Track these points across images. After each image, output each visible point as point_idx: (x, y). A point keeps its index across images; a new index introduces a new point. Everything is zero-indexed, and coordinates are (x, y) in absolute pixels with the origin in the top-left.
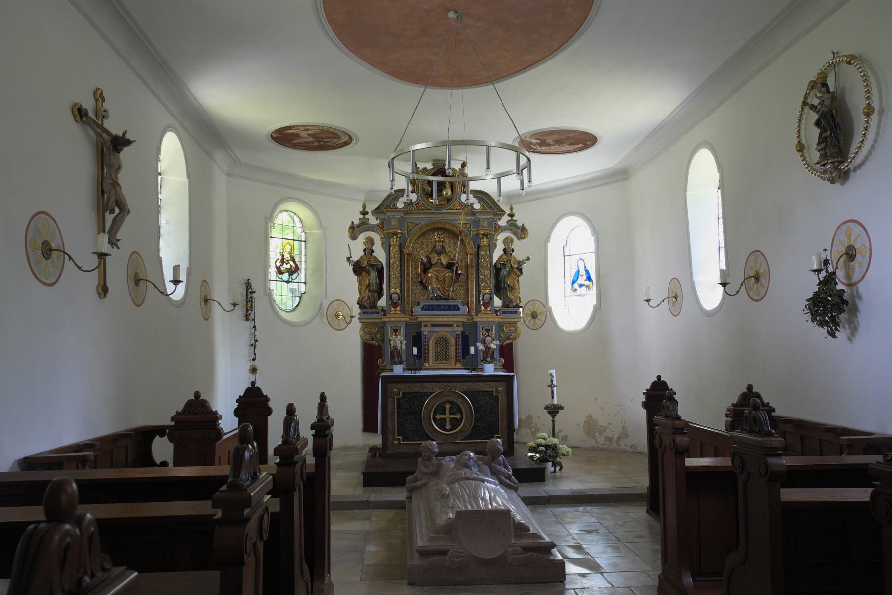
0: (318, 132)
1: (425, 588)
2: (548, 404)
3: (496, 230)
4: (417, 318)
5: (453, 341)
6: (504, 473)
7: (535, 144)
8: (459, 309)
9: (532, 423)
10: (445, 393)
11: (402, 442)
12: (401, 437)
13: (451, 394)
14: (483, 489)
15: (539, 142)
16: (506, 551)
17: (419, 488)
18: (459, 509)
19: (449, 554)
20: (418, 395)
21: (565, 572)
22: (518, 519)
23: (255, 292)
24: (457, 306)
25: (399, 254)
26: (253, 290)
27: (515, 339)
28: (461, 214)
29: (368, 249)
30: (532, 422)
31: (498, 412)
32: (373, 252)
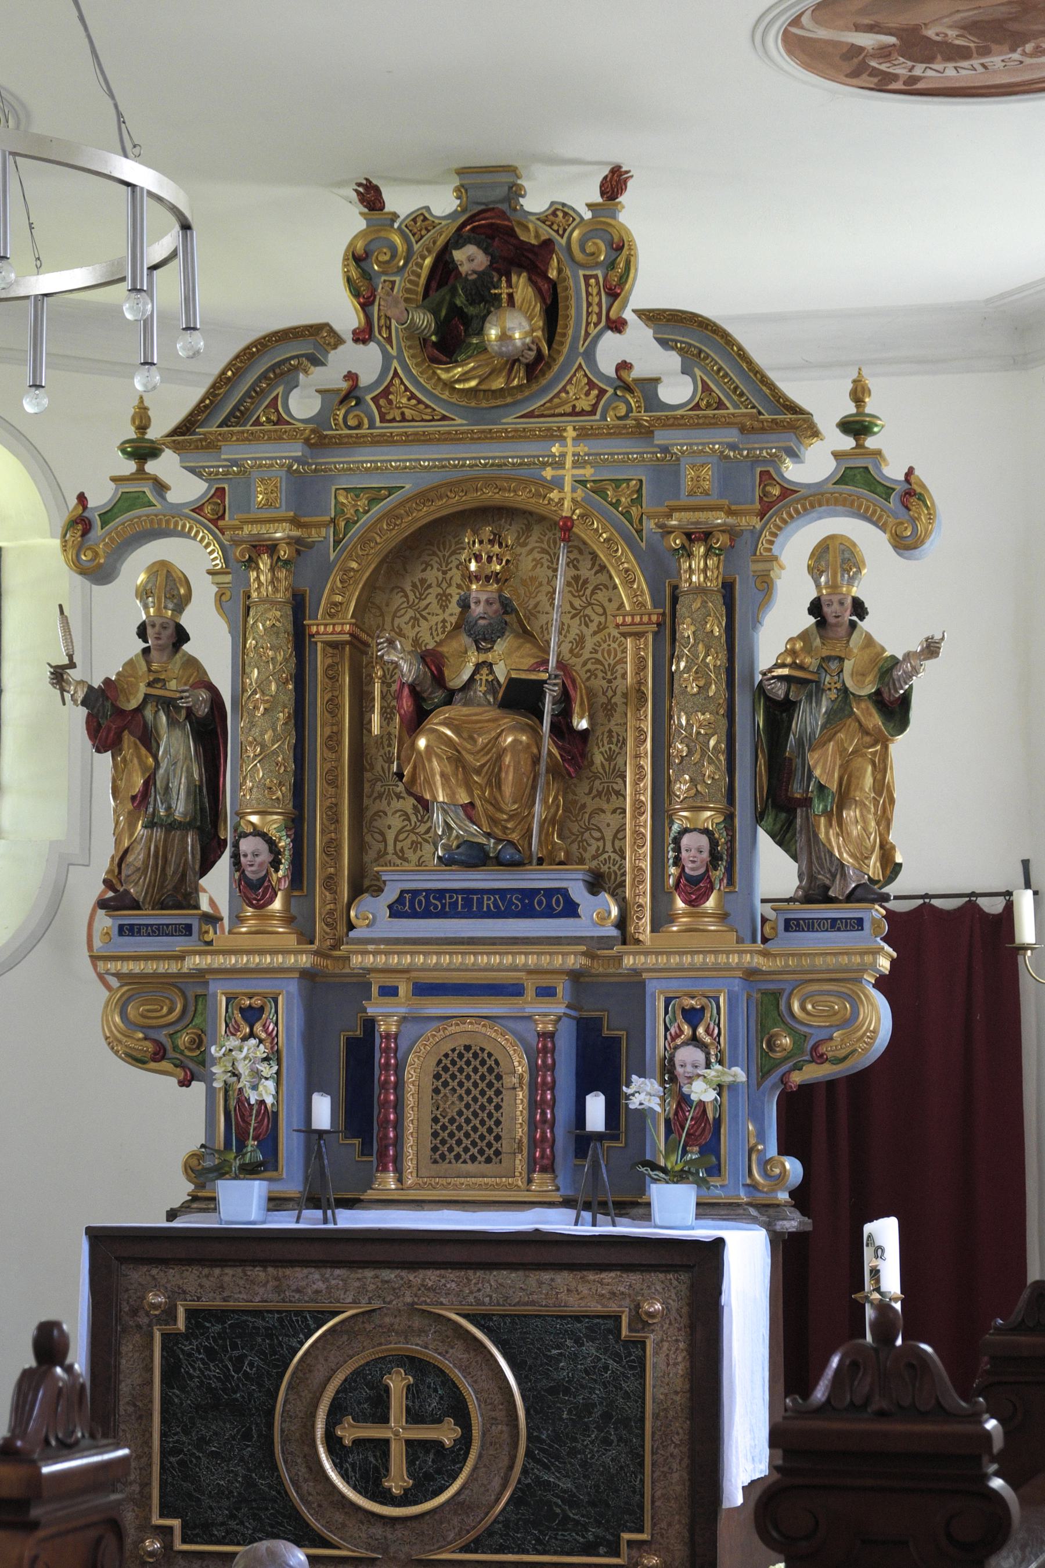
3: (770, 506)
7: (884, 53)
8: (571, 910)
11: (179, 1546)
20: (260, 1323)
24: (564, 892)
25: (289, 648)
29: (153, 626)
32: (181, 636)
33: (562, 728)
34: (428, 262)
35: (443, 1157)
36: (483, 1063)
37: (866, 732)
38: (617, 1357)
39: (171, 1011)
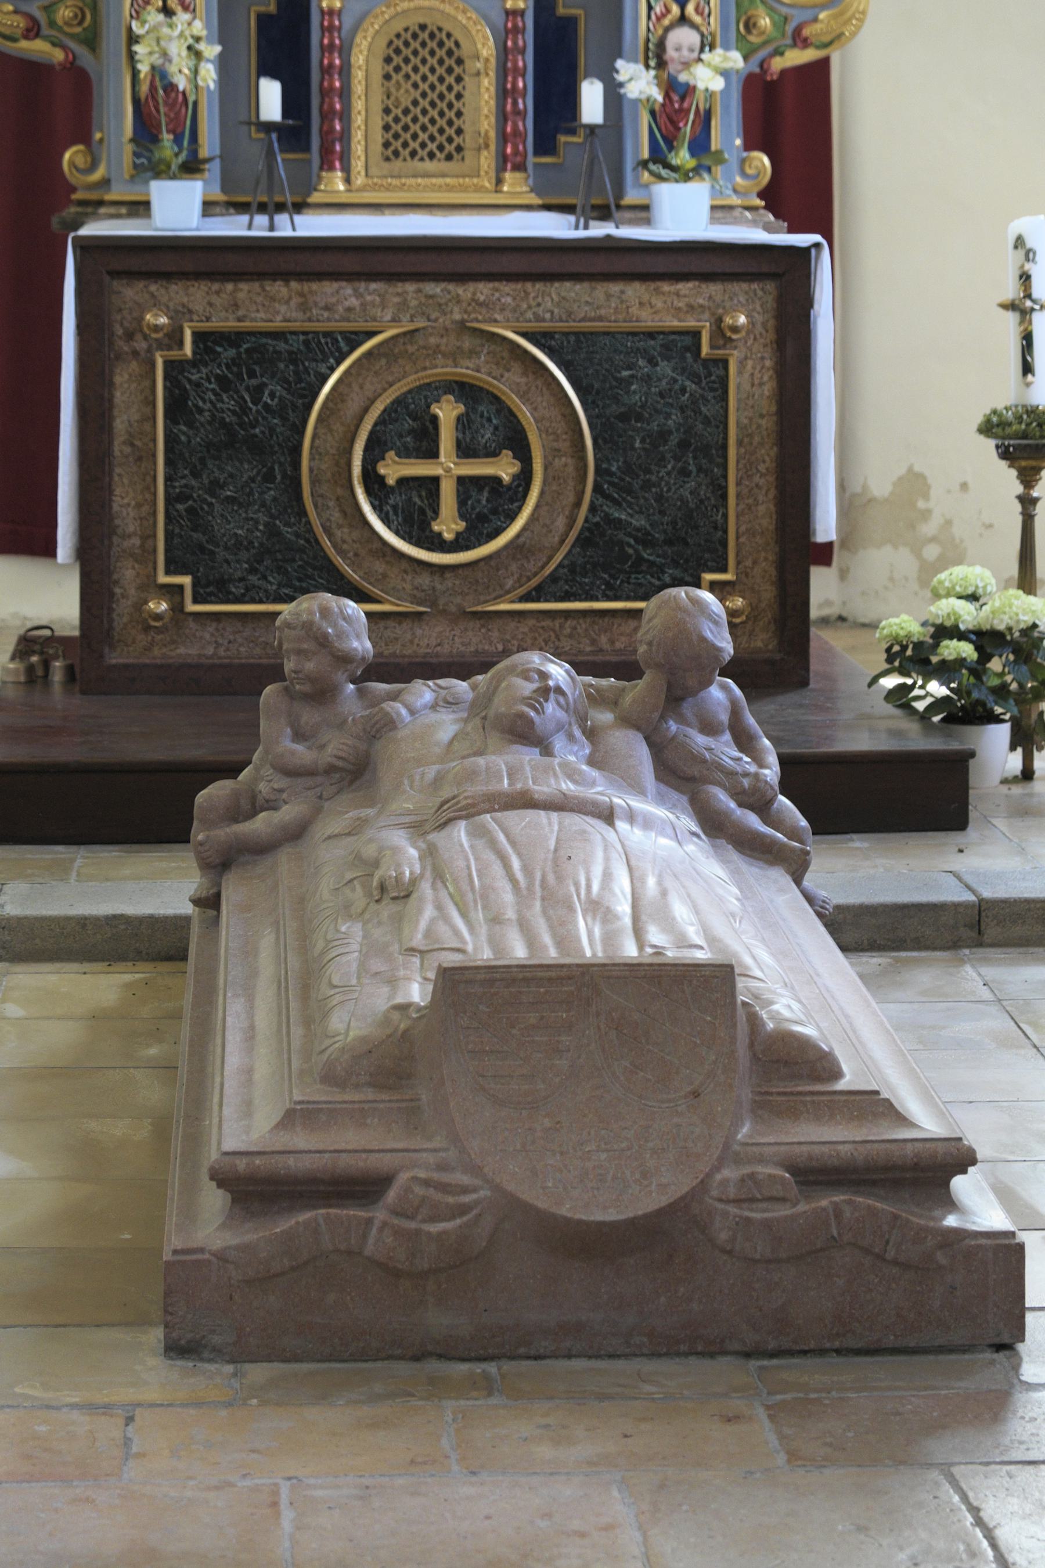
1: (258, 1372)
2: (1000, 406)
5: (487, 49)
6: (731, 774)
9: (926, 515)
10: (432, 340)
11: (191, 607)
12: (186, 580)
13: (467, 343)
14: (600, 854)
16: (704, 1185)
18: (452, 959)
19: (392, 1195)
20: (282, 346)
21: (1024, 1303)
22: (775, 1017)
27: (836, 39)
30: (929, 511)
31: (724, 447)
35: (396, 153)
38: (696, 378)
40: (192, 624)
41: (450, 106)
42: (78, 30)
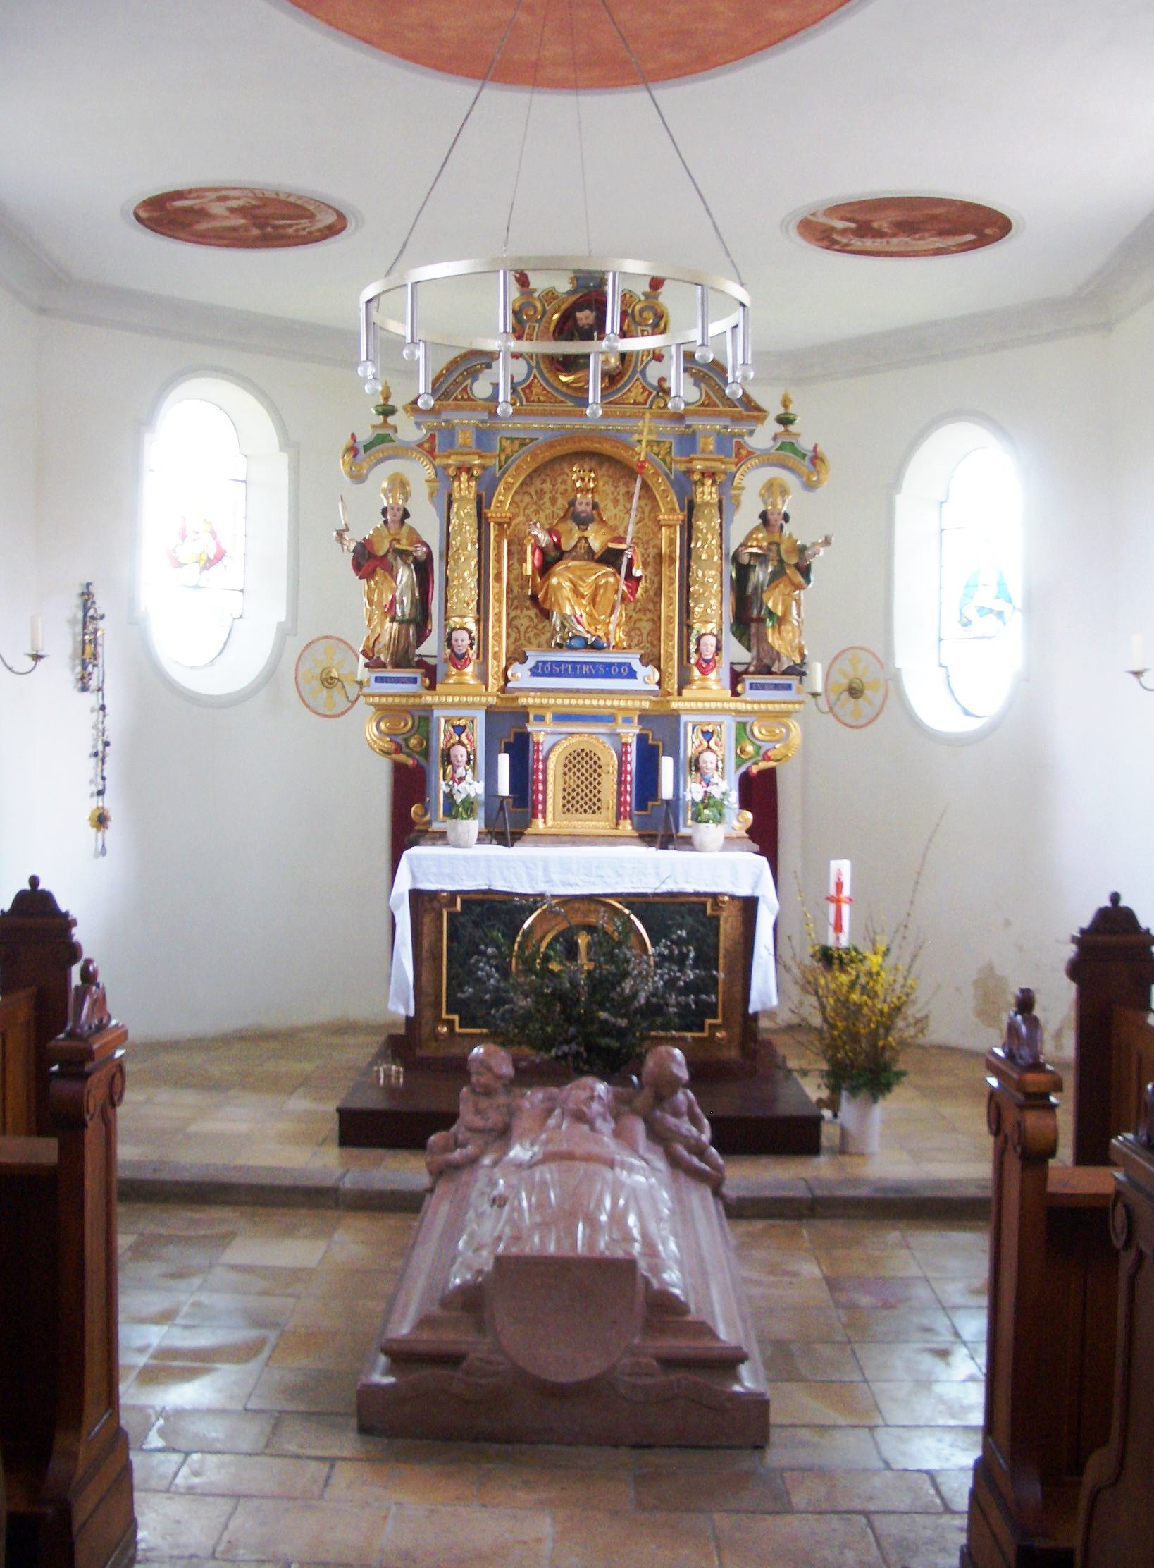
0: (254, 203)
3: (740, 460)
4: (517, 698)
7: (844, 232)
8: (632, 674)
15: (853, 225)
17: (457, 1167)
19: (465, 1364)
23: (102, 617)
24: (629, 665)
26: (100, 612)
28: (642, 416)
33: (629, 575)
34: (556, 316)
35: (568, 810)
36: (591, 758)
37: (793, 584)
38: (703, 925)
39: (405, 725)
40: (459, 1039)
41: (595, 788)
42: (419, 749)
